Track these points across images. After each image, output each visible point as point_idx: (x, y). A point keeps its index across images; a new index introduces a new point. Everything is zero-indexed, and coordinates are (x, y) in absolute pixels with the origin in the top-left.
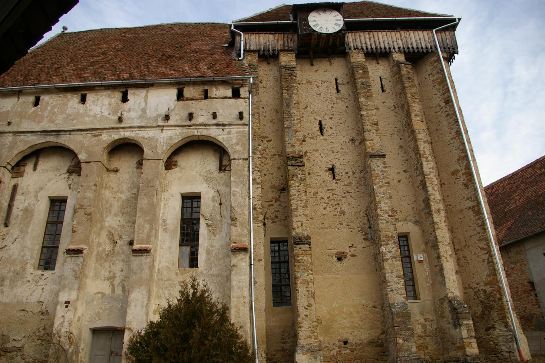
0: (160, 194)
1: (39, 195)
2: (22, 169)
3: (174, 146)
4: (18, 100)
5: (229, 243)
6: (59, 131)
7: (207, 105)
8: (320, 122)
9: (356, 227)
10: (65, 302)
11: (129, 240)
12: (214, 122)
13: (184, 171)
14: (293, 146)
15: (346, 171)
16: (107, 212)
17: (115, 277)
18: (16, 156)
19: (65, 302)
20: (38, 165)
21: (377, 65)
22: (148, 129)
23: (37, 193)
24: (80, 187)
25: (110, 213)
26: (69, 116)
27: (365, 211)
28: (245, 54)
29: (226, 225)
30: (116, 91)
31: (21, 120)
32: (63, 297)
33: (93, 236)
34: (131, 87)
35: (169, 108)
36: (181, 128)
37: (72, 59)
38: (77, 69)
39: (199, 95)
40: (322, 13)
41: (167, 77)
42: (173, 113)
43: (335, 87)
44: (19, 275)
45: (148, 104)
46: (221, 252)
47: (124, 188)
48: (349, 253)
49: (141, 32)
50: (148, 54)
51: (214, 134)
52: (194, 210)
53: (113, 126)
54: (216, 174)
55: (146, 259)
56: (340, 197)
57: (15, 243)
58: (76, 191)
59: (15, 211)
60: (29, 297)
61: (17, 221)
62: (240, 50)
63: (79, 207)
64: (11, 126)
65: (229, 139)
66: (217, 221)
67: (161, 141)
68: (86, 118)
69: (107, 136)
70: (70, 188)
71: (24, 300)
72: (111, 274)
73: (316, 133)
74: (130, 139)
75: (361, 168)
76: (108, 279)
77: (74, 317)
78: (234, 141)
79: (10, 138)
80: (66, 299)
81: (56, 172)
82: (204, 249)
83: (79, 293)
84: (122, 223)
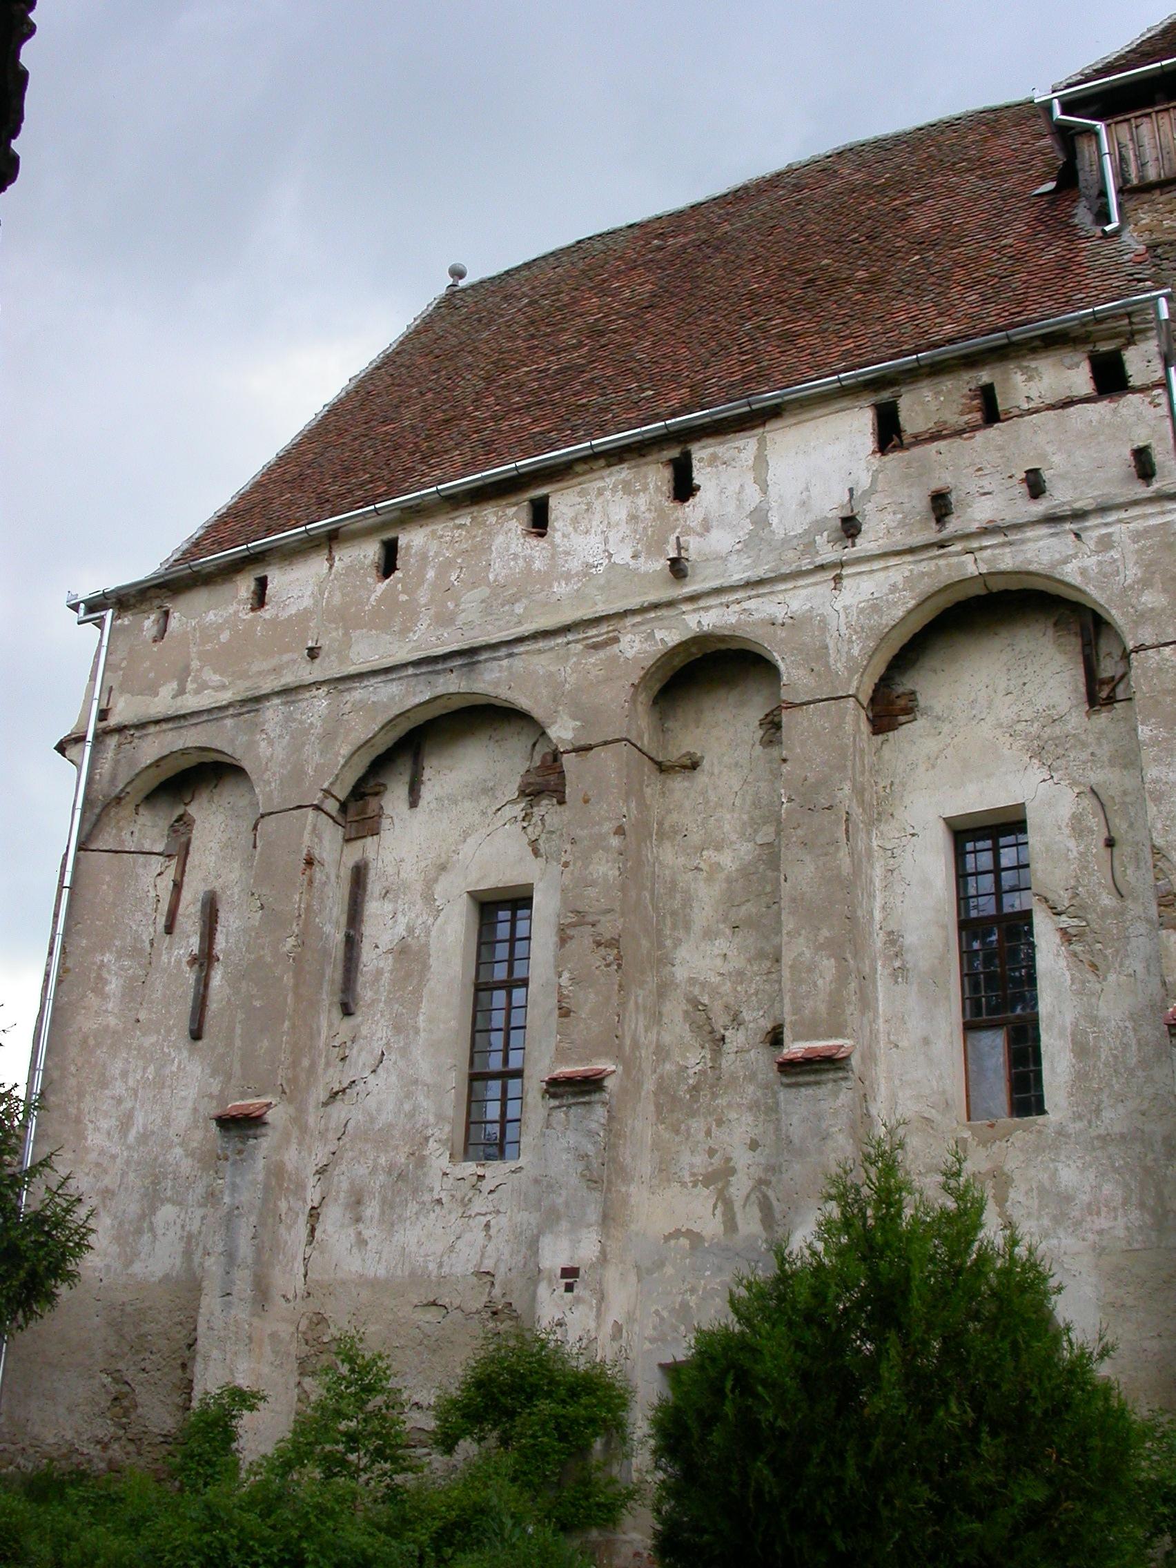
0: (863, 835)
1: (439, 889)
2: (373, 803)
3: (894, 634)
4: (331, 566)
5: (1163, 1000)
6: (472, 651)
7: (1000, 448)
10: (563, 1270)
11: (769, 1026)
12: (1039, 508)
13: (946, 728)
17: (733, 1171)
18: (346, 763)
19: (563, 1270)
20: (422, 782)
22: (782, 587)
23: (430, 883)
24: (568, 847)
25: (687, 927)
26: (498, 588)
28: (1128, 205)
29: (1142, 928)
31: (346, 634)
32: (555, 1255)
33: (636, 1023)
34: (698, 439)
35: (851, 490)
36: (909, 558)
37: (489, 380)
38: (507, 412)
39: (962, 413)
41: (826, 370)
42: (869, 507)
45: (772, 490)
46: (1134, 1041)
47: (727, 827)
49: (719, 217)
50: (753, 297)
51: (1045, 559)
52: (1008, 879)
53: (653, 597)
54: (1077, 719)
55: (836, 1095)
57: (380, 1070)
58: (558, 861)
59: (371, 958)
60: (445, 1258)
62: (1103, 194)
63: (572, 918)
64: (317, 661)
65: (1109, 569)
66: (1105, 914)
67: (838, 623)
68: (556, 584)
69: (637, 639)
70: (536, 853)
71: (432, 1266)
72: (717, 1161)
74: (723, 638)
76: (709, 1179)
77: (599, 1326)
78: (1132, 572)
79: (318, 705)
80: (563, 1261)
81: (485, 801)
83: (608, 1237)
84: (737, 962)
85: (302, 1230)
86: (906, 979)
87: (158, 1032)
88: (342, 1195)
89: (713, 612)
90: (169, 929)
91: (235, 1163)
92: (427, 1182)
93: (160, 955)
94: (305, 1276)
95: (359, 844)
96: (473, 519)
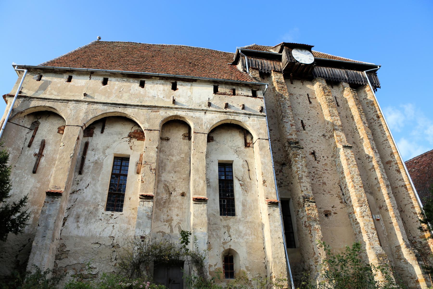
8: (302, 121)
9: (334, 194)
11: (182, 192)
13: (219, 144)
14: (291, 135)
15: (323, 155)
16: (162, 169)
21: (332, 89)
25: (165, 170)
27: (338, 184)
30: (168, 82)
34: (179, 81)
35: (209, 98)
40: (300, 50)
43: (308, 100)
44: (92, 214)
48: (333, 212)
56: (321, 173)
60: (101, 232)
61: (88, 170)
66: (248, 182)
70: (131, 149)
71: (98, 234)
73: (300, 128)
74: (180, 117)
75: (332, 154)
81: (119, 136)
82: (240, 202)
85: (62, 223)
86: (210, 188)
87: (22, 170)
88: (74, 215)
89: (180, 112)
90: (29, 146)
91: (50, 204)
92: (98, 215)
93: (25, 152)
94: (61, 234)
95: (87, 138)
96: (127, 80)
